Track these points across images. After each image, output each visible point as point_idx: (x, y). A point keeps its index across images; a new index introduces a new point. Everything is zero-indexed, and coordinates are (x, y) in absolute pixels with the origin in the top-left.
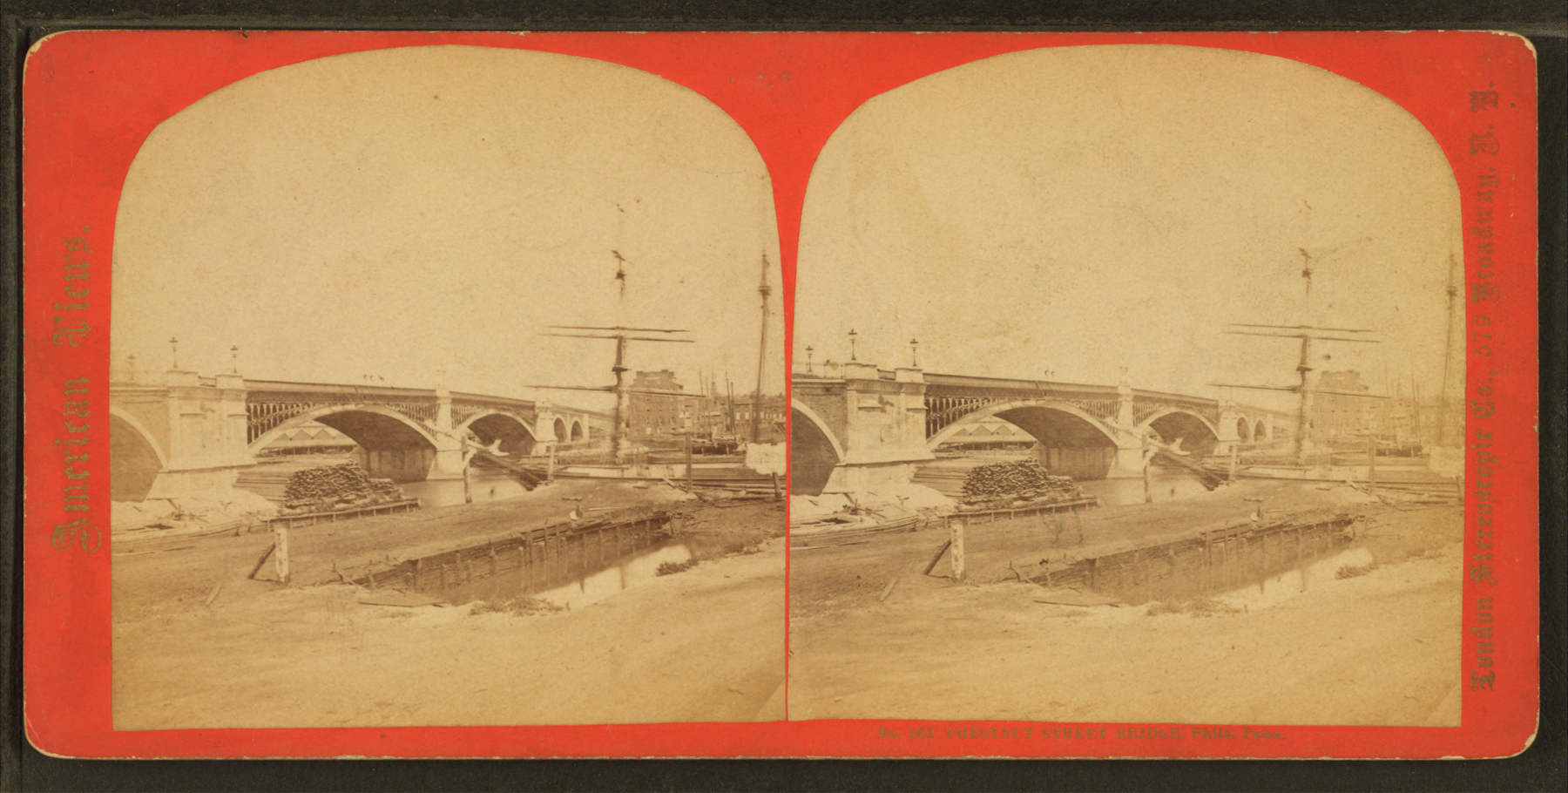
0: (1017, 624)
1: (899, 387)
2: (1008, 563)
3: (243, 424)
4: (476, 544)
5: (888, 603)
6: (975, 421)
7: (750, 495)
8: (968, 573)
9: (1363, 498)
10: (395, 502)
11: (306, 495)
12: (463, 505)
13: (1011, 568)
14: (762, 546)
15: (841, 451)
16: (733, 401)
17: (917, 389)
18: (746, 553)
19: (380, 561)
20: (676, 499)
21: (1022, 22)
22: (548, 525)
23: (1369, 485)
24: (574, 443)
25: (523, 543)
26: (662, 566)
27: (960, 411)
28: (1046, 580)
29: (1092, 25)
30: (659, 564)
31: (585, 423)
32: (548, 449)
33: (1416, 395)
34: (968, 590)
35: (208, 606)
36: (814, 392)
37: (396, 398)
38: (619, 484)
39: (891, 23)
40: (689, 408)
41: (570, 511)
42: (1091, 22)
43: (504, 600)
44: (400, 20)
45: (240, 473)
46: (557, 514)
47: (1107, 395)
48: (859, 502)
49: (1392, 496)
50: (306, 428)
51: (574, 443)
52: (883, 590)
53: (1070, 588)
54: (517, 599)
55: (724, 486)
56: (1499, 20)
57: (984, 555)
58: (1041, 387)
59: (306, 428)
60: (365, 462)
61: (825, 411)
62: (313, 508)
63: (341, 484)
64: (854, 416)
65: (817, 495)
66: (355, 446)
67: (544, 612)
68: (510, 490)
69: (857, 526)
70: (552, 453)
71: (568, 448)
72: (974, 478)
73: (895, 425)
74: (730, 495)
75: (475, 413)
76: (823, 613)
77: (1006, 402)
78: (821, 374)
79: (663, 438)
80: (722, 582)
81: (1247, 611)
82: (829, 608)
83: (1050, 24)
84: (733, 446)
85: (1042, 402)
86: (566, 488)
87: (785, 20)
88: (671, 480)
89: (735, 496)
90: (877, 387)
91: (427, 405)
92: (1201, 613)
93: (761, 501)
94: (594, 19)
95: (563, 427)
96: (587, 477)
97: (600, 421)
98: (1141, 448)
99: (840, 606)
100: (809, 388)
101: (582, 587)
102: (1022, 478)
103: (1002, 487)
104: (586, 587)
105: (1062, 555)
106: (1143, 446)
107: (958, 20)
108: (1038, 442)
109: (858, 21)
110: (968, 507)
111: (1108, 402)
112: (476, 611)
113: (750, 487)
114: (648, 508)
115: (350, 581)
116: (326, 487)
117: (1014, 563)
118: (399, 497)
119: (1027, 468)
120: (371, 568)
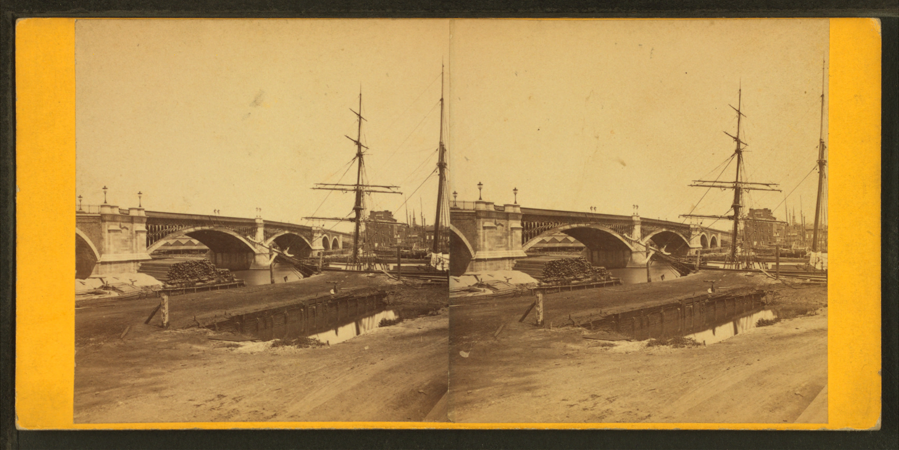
0: (573, 350)
1: (132, 220)
2: (568, 316)
3: (144, 236)
4: (652, 306)
5: (125, 340)
6: (550, 235)
7: (813, 282)
8: (170, 323)
9: (771, 281)
10: (607, 280)
11: (179, 277)
12: (646, 283)
13: (570, 319)
14: (818, 311)
15: (473, 251)
16: (804, 227)
17: (142, 220)
18: (809, 315)
19: (219, 314)
20: (769, 283)
21: (585, 11)
22: (695, 296)
23: (776, 272)
24: (712, 249)
25: (304, 307)
26: (759, 321)
27: (541, 229)
28: (590, 325)
29: (625, 12)
30: (758, 320)
31: (341, 240)
32: (697, 252)
33: (803, 223)
34: (171, 332)
35: (121, 339)
36: (83, 221)
37: (609, 221)
38: (359, 275)
39: (511, 12)
40: (779, 231)
41: (331, 289)
42: (625, 11)
43: (667, 338)
44: (231, 13)
45: (141, 264)
46: (323, 291)
47: (625, 221)
48: (108, 283)
49: (788, 280)
50: (182, 238)
51: (712, 249)
52: (122, 332)
53: (604, 330)
54: (299, 338)
55: (798, 276)
56: (858, 8)
57: (180, 313)
58: (212, 219)
59: (182, 238)
60: (214, 259)
61: (89, 232)
62: (184, 284)
63: (200, 272)
64: (106, 235)
65: (84, 279)
66: (208, 250)
67: (690, 346)
68: (672, 275)
69: (107, 296)
70: (321, 257)
71: (329, 254)
72: (174, 270)
73: (129, 240)
74: (801, 281)
75: (277, 233)
76: (88, 345)
77: (568, 225)
78: (87, 211)
79: (384, 249)
80: (417, 331)
81: (705, 344)
82: (92, 342)
83: (602, 12)
84: (804, 253)
85: (589, 224)
86: (706, 275)
87: (450, 11)
88: (767, 272)
89: (804, 282)
90: (119, 219)
91: (250, 228)
92: (679, 345)
93: (819, 286)
94: (342, 11)
95: (706, 241)
96: (717, 269)
97: (727, 237)
98: (268, 254)
99: (98, 341)
100: (455, 215)
101: (337, 333)
102: (201, 270)
103: (565, 273)
104: (339, 333)
105: (599, 311)
106: (270, 252)
107: (549, 10)
108: (210, 250)
109: (492, 11)
110: (171, 286)
111: (626, 225)
112: (651, 344)
113: (812, 277)
114: (753, 289)
115: (204, 326)
116: (191, 273)
117: (572, 315)
118: (609, 278)
119: (579, 262)
120: (216, 319)
